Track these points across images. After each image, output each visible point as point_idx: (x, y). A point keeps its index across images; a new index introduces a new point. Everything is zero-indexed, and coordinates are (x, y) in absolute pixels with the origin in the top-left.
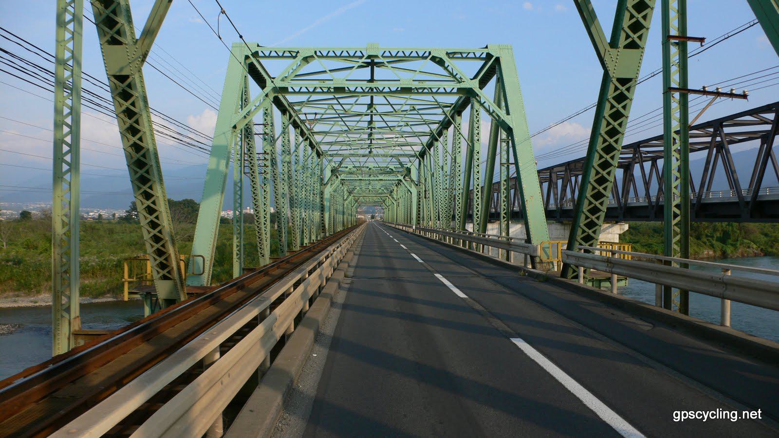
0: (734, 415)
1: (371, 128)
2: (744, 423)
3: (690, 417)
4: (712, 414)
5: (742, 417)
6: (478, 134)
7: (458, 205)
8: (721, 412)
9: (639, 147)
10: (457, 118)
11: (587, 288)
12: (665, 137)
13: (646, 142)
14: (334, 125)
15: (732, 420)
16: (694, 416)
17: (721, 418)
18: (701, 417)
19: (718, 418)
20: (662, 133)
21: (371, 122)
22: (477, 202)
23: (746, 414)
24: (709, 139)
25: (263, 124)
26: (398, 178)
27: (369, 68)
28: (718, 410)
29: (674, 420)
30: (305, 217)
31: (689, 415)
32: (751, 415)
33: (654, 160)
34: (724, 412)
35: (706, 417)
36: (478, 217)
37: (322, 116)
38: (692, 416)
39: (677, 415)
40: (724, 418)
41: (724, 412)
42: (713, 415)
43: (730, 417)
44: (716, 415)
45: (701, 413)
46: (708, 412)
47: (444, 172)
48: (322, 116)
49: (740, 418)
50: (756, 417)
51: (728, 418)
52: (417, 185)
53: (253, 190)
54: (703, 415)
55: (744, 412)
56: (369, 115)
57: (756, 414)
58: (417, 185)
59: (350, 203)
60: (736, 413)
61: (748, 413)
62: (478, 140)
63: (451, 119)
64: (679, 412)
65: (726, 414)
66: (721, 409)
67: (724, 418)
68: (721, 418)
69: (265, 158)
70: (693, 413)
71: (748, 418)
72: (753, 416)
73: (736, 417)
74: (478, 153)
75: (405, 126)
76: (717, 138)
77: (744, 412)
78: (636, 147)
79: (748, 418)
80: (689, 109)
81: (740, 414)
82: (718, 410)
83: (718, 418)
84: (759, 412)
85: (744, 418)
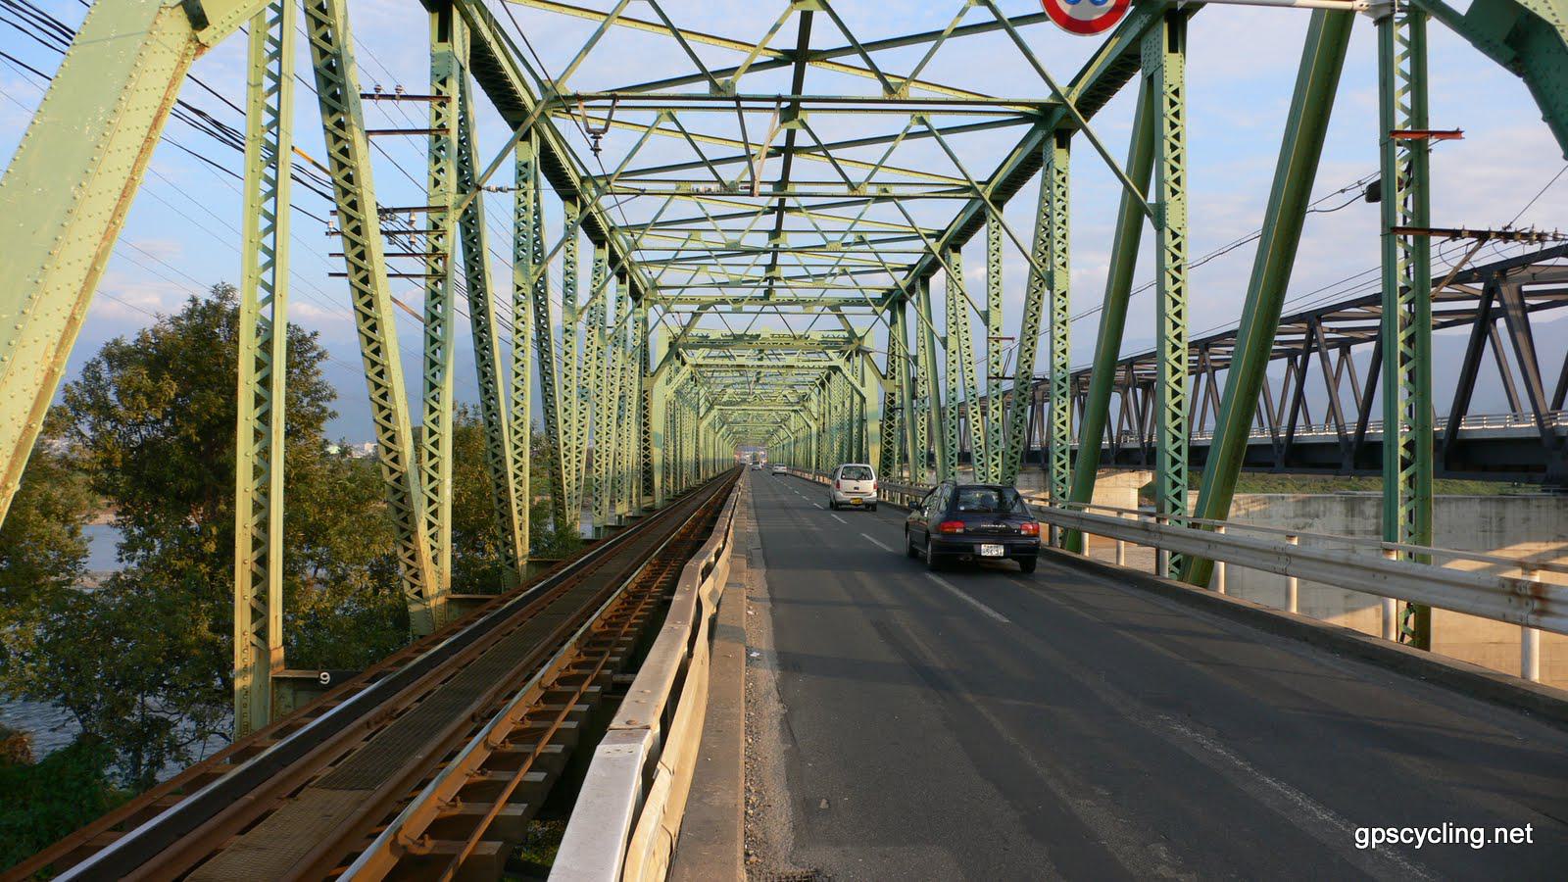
0: (1477, 835)
1: (771, 279)
2: (1497, 852)
3: (1388, 840)
4: (1434, 833)
5: (1493, 839)
6: (1064, 250)
7: (1059, 416)
8: (1451, 830)
9: (1320, 320)
10: (954, 257)
11: (1290, 618)
12: (1385, 297)
13: (1332, 312)
14: (697, 271)
15: (1472, 845)
16: (1397, 837)
17: (1451, 841)
18: (1412, 839)
19: (1445, 841)
20: (1379, 290)
21: (771, 267)
22: (1059, 417)
23: (1501, 834)
24: (1475, 304)
25: (429, 131)
26: (832, 364)
27: (812, 46)
28: (1445, 825)
29: (1357, 845)
30: (597, 447)
31: (1387, 836)
32: (1512, 835)
33: (1344, 346)
34: (1458, 831)
35: (1421, 840)
36: (923, 448)
37: (676, 255)
38: (1393, 839)
39: (1362, 835)
40: (1457, 841)
41: (1458, 831)
42: (1435, 835)
43: (1470, 841)
44: (1441, 835)
45: (1411, 831)
46: (1425, 830)
47: (992, 329)
48: (676, 255)
49: (1489, 841)
50: (1521, 840)
51: (1466, 841)
52: (885, 377)
53: (367, 351)
54: (1414, 835)
55: (1497, 831)
56: (769, 252)
57: (1522, 834)
58: (885, 377)
59: (712, 425)
60: (1481, 831)
61: (1505, 831)
62: (1064, 265)
63: (939, 257)
64: (1366, 831)
65: (1462, 833)
66: (1451, 824)
67: (1457, 841)
68: (1451, 841)
69: (435, 249)
70: (1396, 831)
71: (1506, 841)
72: (1516, 838)
73: (1481, 840)
74: (1064, 294)
75: (841, 275)
76: (1494, 302)
77: (1497, 831)
78: (1312, 319)
79: (1506, 841)
80: (1431, 249)
81: (1489, 835)
82: (1445, 825)
83: (1445, 841)
84: (1529, 829)
85: (1497, 841)
